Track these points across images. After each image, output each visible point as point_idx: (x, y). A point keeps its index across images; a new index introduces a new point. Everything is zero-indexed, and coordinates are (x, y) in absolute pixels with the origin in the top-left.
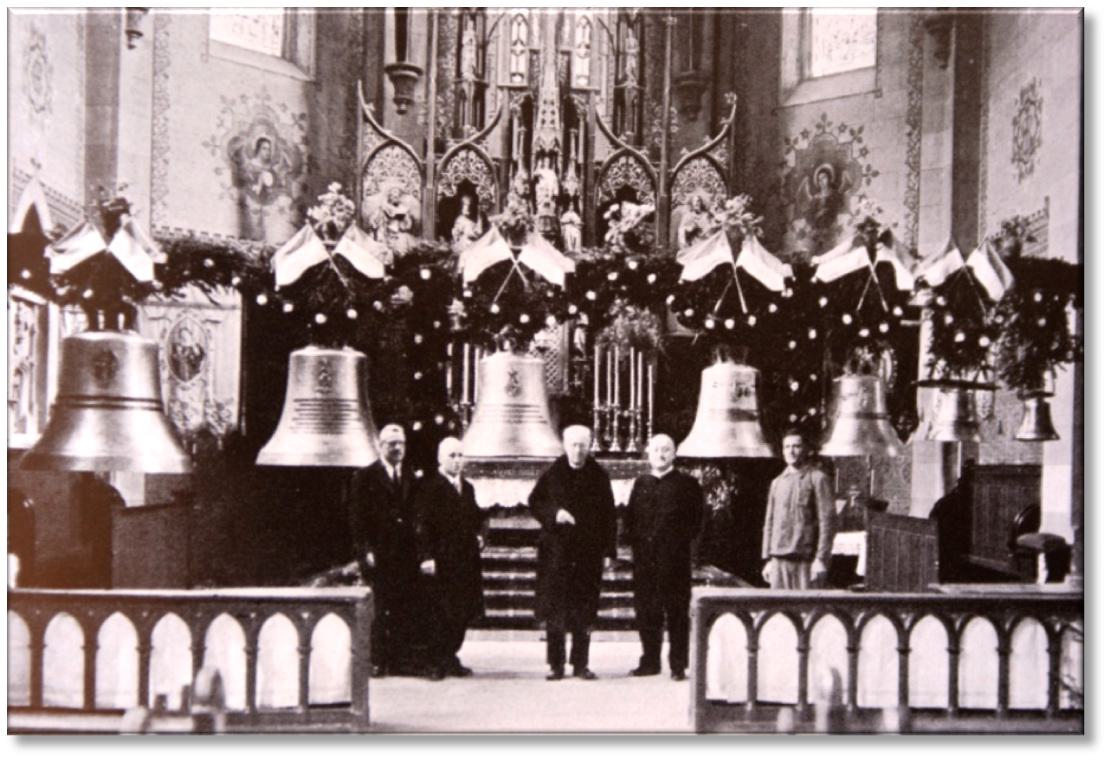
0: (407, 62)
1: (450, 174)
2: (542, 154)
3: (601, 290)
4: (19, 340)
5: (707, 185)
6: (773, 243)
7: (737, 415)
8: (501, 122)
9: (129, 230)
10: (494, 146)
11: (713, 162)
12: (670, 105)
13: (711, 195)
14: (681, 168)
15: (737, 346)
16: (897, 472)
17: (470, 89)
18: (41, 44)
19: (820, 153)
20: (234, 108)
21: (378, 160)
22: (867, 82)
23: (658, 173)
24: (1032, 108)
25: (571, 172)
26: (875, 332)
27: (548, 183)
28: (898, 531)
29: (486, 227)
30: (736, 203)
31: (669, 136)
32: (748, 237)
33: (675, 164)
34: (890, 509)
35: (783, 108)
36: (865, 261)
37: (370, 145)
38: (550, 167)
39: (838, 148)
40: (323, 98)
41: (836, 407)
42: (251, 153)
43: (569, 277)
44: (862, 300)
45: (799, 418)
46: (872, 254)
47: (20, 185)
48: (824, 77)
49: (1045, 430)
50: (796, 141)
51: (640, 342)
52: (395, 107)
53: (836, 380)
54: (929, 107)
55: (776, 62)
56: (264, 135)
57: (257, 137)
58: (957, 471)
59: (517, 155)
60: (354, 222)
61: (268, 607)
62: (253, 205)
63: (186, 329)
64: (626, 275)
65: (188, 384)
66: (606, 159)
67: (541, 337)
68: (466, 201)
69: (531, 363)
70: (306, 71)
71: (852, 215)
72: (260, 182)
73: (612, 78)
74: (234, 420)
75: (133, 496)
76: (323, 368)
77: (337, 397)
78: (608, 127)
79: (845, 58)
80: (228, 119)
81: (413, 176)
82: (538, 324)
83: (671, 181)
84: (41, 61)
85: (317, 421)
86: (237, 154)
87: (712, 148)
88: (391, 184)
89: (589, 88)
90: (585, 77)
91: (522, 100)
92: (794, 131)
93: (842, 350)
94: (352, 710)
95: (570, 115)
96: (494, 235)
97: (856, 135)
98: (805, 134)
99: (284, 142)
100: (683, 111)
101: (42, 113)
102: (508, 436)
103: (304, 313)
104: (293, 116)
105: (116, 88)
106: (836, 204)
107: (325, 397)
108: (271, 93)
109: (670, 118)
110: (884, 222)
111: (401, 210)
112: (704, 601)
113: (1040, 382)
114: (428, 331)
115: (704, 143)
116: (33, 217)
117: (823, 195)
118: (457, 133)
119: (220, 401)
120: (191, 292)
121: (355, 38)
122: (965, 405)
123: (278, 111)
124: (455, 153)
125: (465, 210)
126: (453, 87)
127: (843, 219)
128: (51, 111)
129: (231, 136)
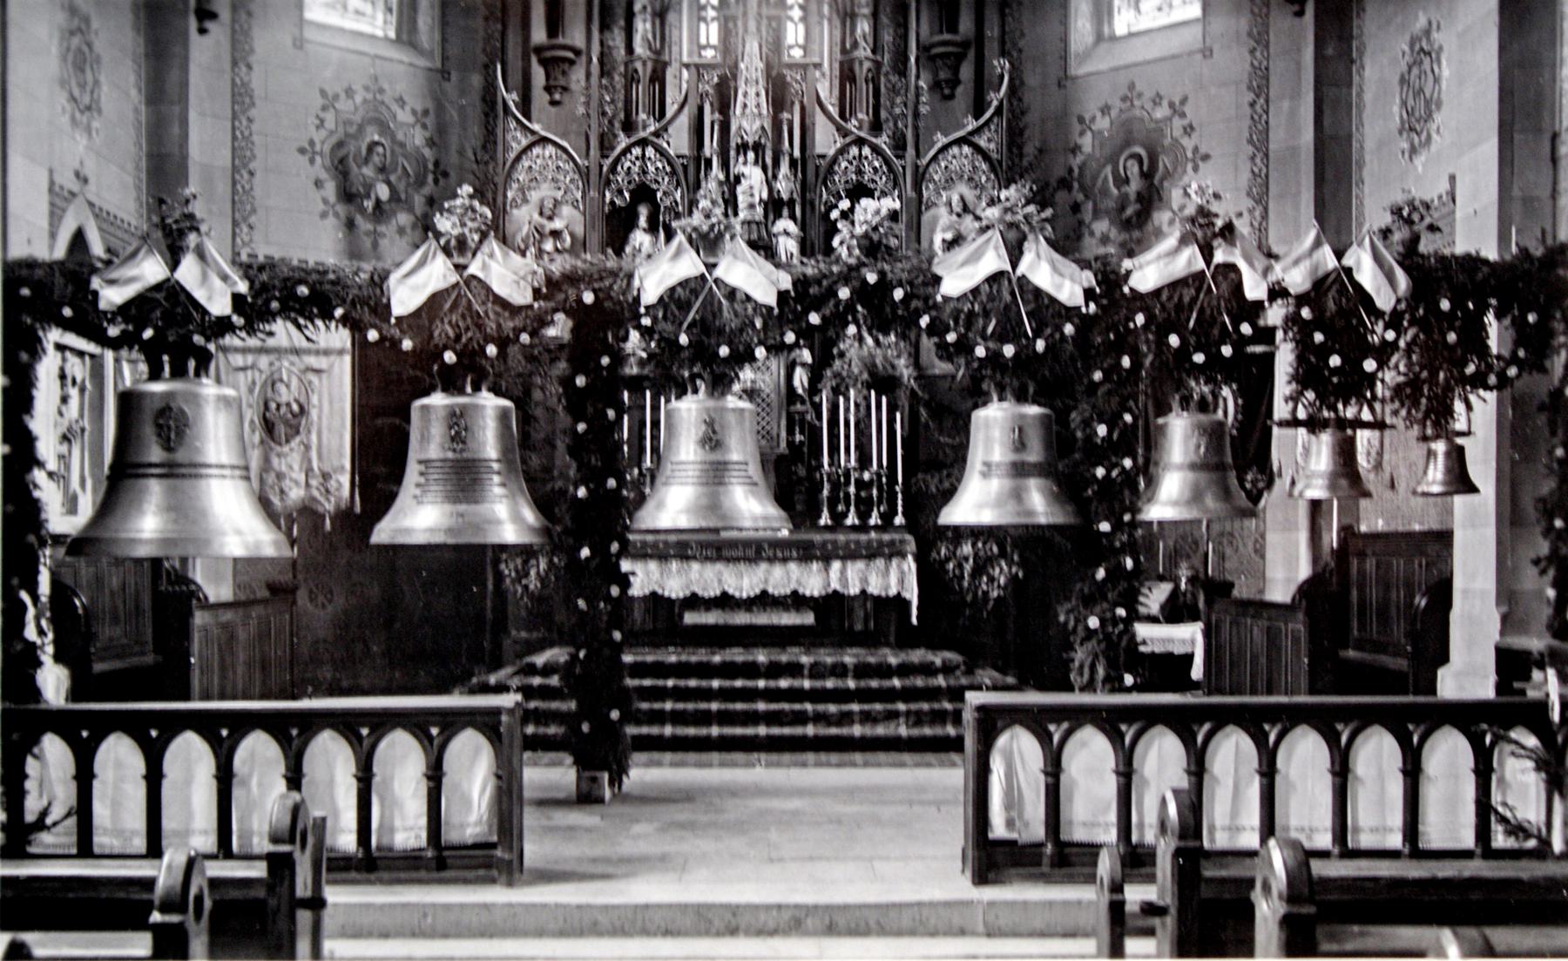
0: (561, 40)
2: (743, 148)
3: (827, 312)
4: (65, 399)
5: (971, 179)
6: (1066, 245)
7: (1019, 470)
8: (686, 110)
9: (201, 254)
10: (678, 141)
11: (977, 149)
12: (918, 77)
13: (978, 192)
14: (935, 158)
16: (1245, 545)
17: (645, 70)
18: (83, 27)
19: (1127, 135)
20: (337, 105)
21: (526, 163)
22: (1193, 36)
23: (904, 168)
24: (1427, 61)
25: (784, 168)
26: (1214, 357)
27: (753, 177)
28: (1249, 621)
29: (670, 236)
30: (1011, 193)
31: (916, 115)
32: (1031, 237)
33: (926, 154)
34: (1236, 593)
35: (1075, 78)
36: (1200, 264)
37: (514, 145)
38: (756, 162)
39: (1153, 125)
40: (451, 87)
42: (359, 162)
43: (782, 296)
44: (1194, 315)
45: (1109, 472)
46: (1207, 253)
47: (63, 204)
48: (1131, 35)
49: (1460, 481)
50: (1093, 119)
51: (883, 382)
52: (547, 97)
53: (1160, 421)
54: (1279, 69)
56: (376, 138)
57: (368, 140)
58: (1332, 538)
59: (710, 148)
60: (492, 233)
61: (384, 722)
62: (363, 225)
63: (281, 380)
64: (863, 292)
65: (286, 449)
66: (832, 152)
67: (747, 374)
68: (643, 213)
70: (428, 55)
71: (1173, 212)
72: (373, 196)
73: (837, 49)
74: (346, 492)
75: (218, 590)
76: (455, 420)
77: (476, 456)
78: (834, 111)
79: (1160, 9)
80: (330, 118)
81: (572, 181)
82: (744, 356)
83: (920, 178)
84: (85, 49)
85: (449, 488)
87: (977, 131)
88: (544, 192)
89: (808, 60)
90: (800, 47)
91: (716, 80)
92: (1091, 108)
94: (499, 853)
95: (779, 97)
96: (680, 244)
98: (1105, 110)
99: (402, 145)
100: (936, 86)
101: (87, 114)
102: (704, 501)
104: (414, 112)
105: (185, 84)
106: (1150, 199)
107: (458, 456)
108: (386, 86)
109: (918, 95)
110: (1222, 212)
111: (558, 224)
112: (982, 709)
113: (1449, 412)
114: (593, 371)
115: (964, 126)
116: (79, 239)
117: (1135, 186)
118: (629, 126)
119: (327, 468)
120: (282, 331)
121: (492, 13)
122: (1345, 453)
123: (395, 107)
124: (627, 150)
125: (643, 221)
126: (622, 69)
127: (1161, 217)
128: (100, 111)
129: (334, 140)
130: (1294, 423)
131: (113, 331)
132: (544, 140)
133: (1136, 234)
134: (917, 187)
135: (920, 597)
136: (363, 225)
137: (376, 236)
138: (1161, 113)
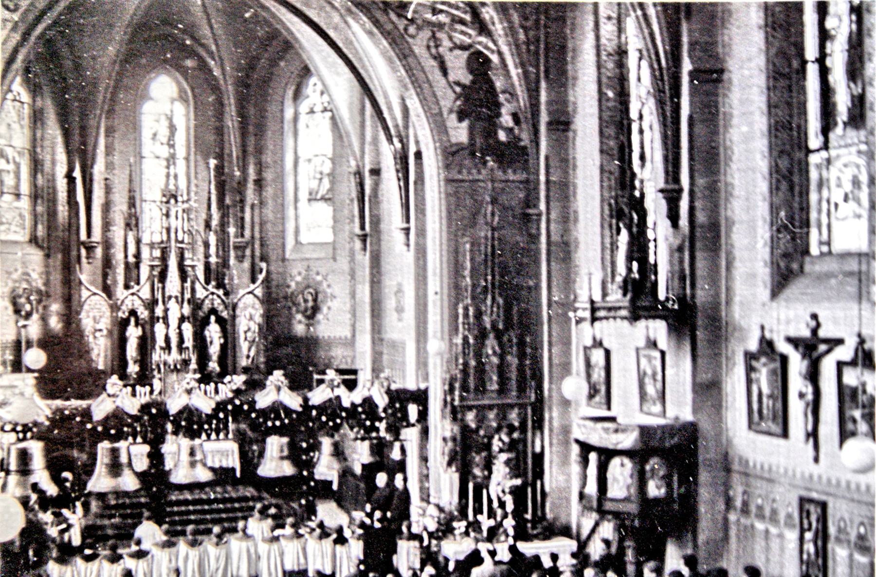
2: (170, 297)
10: (146, 293)
11: (255, 296)
25: (186, 304)
40: (51, 261)
68: (133, 320)
86: (14, 298)
117: (310, 304)
130: (356, 439)
132: (95, 294)
133: (311, 321)
135: (241, 463)
138: (319, 278)
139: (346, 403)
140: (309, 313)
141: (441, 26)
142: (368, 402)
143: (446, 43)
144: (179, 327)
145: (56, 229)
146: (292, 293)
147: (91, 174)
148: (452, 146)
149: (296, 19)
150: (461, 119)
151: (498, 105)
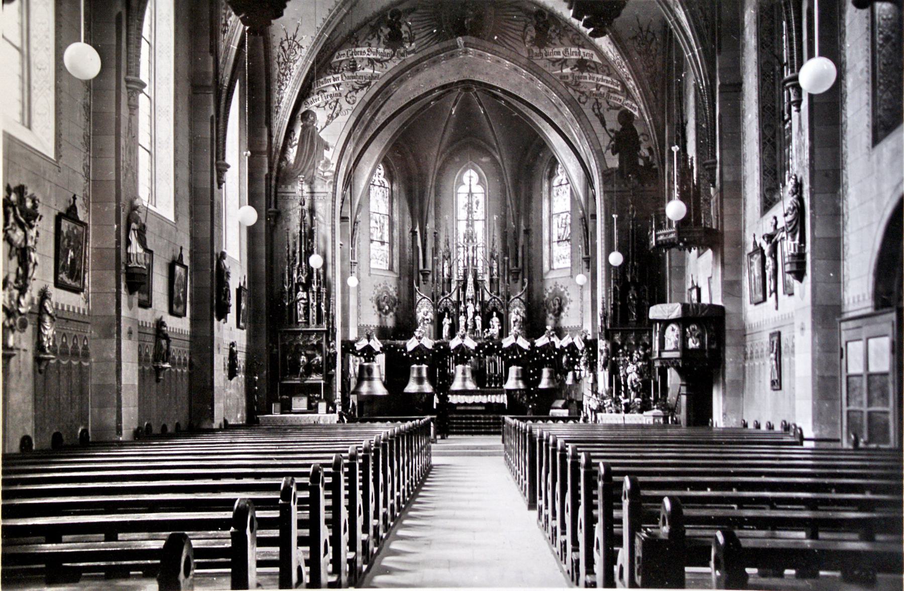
1: (441, 306)
2: (468, 300)
7: (517, 379)
10: (454, 298)
15: (516, 362)
25: (478, 305)
40: (401, 282)
41: (745, 316)
43: (476, 347)
46: (550, 339)
48: (558, 269)
55: (542, 266)
59: (461, 299)
69: (468, 366)
70: (397, 274)
78: (489, 291)
80: (376, 291)
83: (508, 306)
93: (541, 364)
97: (566, 289)
98: (551, 288)
103: (414, 357)
111: (428, 317)
117: (557, 306)
118: (443, 294)
125: (446, 316)
131: (359, 354)
134: (507, 309)
136: (383, 316)
137: (386, 318)
138: (562, 290)
139: (558, 346)
140: (557, 312)
141: (601, 95)
142: (572, 346)
143: (605, 105)
144: (474, 318)
145: (405, 263)
146: (546, 301)
147: (426, 230)
148: (608, 169)
149: (534, 114)
150: (614, 154)
151: (639, 143)
